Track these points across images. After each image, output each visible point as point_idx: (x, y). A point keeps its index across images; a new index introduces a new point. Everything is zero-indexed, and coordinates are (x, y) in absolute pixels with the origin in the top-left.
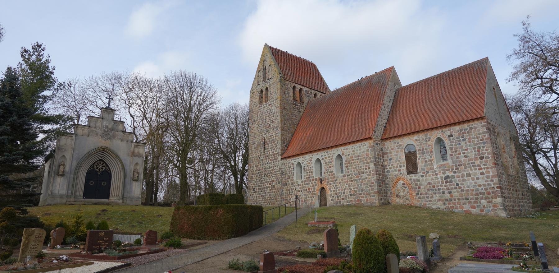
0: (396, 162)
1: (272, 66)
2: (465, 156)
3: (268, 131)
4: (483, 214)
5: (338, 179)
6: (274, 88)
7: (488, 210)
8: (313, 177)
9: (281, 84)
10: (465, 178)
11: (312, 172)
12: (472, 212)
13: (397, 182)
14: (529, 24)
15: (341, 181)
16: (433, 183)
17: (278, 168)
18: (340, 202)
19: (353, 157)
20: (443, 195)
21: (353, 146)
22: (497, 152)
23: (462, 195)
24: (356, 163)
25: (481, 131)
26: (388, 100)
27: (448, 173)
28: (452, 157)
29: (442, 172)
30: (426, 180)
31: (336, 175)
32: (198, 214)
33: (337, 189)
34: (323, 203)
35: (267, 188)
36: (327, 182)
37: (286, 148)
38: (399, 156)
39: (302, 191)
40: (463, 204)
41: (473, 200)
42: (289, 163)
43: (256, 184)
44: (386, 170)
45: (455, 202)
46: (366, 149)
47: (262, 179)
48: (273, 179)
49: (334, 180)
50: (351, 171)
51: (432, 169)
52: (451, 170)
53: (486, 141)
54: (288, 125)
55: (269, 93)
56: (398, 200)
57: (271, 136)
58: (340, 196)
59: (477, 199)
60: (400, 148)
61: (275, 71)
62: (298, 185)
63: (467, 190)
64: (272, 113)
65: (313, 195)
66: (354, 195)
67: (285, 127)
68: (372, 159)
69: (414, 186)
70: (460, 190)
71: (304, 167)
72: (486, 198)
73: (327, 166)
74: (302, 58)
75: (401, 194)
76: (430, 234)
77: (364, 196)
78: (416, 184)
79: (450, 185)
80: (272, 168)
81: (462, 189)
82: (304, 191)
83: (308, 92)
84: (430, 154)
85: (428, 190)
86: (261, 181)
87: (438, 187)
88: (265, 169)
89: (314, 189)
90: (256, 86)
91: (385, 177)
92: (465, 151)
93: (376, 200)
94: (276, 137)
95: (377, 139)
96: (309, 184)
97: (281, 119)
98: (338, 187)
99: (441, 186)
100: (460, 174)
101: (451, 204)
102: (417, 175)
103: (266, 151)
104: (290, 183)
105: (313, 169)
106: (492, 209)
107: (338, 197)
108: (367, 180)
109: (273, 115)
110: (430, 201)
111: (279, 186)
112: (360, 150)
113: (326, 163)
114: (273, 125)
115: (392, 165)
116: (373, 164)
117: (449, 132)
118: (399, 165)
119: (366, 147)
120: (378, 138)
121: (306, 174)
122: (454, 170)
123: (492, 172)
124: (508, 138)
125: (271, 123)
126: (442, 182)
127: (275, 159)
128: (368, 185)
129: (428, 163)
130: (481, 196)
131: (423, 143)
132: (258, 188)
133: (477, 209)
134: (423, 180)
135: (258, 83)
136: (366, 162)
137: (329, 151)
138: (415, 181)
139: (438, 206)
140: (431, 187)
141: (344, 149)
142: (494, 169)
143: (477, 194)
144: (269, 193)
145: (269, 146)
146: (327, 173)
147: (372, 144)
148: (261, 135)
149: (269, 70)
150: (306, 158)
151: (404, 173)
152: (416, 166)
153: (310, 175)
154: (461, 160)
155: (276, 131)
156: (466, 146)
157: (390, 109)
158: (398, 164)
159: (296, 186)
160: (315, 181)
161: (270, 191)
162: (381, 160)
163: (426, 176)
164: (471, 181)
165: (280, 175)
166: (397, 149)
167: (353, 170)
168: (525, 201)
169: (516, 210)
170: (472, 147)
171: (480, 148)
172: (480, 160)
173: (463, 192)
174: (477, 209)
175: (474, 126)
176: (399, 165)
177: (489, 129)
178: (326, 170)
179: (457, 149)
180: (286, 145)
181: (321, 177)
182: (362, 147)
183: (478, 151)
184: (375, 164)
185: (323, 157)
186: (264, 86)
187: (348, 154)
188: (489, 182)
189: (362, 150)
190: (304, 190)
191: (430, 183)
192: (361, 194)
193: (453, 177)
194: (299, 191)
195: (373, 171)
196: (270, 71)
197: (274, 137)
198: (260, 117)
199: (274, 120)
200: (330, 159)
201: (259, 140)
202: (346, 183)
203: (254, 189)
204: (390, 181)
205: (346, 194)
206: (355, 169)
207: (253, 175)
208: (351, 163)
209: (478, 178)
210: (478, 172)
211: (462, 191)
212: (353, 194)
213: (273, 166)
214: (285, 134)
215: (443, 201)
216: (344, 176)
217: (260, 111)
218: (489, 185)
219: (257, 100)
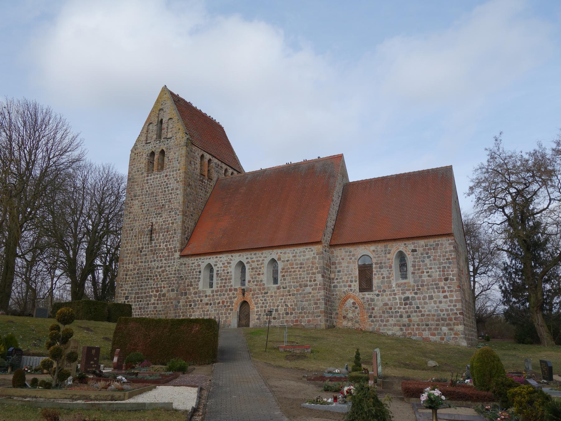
0: (346, 275)
2: (429, 276)
3: (159, 214)
4: (443, 343)
5: (269, 292)
6: (175, 153)
7: (449, 338)
8: (231, 286)
9: (188, 149)
10: (427, 301)
11: (230, 279)
12: (432, 340)
13: (345, 301)
14: (501, 140)
15: (273, 294)
16: (389, 304)
17: (174, 269)
18: (270, 322)
20: (400, 319)
21: (294, 250)
23: (422, 320)
24: (297, 272)
25: (447, 250)
27: (408, 294)
29: (401, 292)
30: (382, 301)
31: (266, 286)
34: (244, 322)
35: (151, 296)
36: (253, 295)
38: (350, 268)
39: (211, 304)
40: (423, 331)
41: (434, 327)
42: (193, 264)
43: (132, 290)
45: (414, 328)
46: (313, 255)
47: (142, 283)
49: (263, 292)
50: (290, 282)
51: (390, 287)
52: (411, 291)
55: (166, 159)
56: (345, 323)
57: (164, 222)
59: (438, 325)
60: (353, 258)
61: (179, 129)
62: (206, 296)
63: (428, 315)
65: (229, 311)
66: (292, 314)
67: (188, 212)
68: (319, 269)
70: (420, 314)
72: (448, 325)
73: (254, 273)
74: (208, 115)
75: (350, 315)
76: (428, 362)
77: (305, 316)
78: (369, 305)
80: (163, 269)
81: (423, 313)
83: (218, 165)
84: (389, 270)
85: (384, 312)
86: (141, 286)
87: (396, 309)
88: (150, 268)
89: (232, 303)
91: (331, 292)
92: (429, 270)
94: (173, 223)
96: (224, 295)
97: (184, 199)
98: (268, 301)
99: (399, 308)
100: (422, 296)
101: (409, 330)
102: (372, 293)
103: (153, 242)
105: (231, 275)
106: (453, 338)
108: (310, 295)
109: (170, 192)
110: (385, 325)
111: (172, 295)
113: (252, 269)
114: (169, 207)
115: (341, 278)
116: (320, 275)
117: (413, 246)
118: (350, 279)
119: (312, 253)
120: (327, 244)
122: (415, 290)
126: (401, 304)
127: (169, 256)
128: (312, 302)
129: (386, 280)
130: (443, 322)
131: (381, 256)
132: (133, 296)
133: (437, 336)
134: (378, 300)
135: (147, 140)
136: (311, 272)
137: (259, 253)
138: (368, 301)
139: (393, 332)
140: (388, 309)
141: (281, 253)
142: (458, 293)
143: (438, 320)
144: (154, 304)
145: (159, 236)
146: (253, 282)
148: (147, 219)
150: (222, 259)
151: (355, 290)
153: (225, 283)
154: (424, 280)
156: (430, 264)
157: (338, 208)
158: (348, 278)
159: (202, 297)
160: (233, 291)
161: (156, 302)
164: (433, 304)
165: (176, 280)
166: (348, 260)
167: (292, 281)
170: (437, 266)
171: (445, 268)
172: (444, 282)
173: (424, 316)
174: (437, 336)
176: (349, 280)
178: (252, 278)
179: (420, 266)
180: (187, 240)
181: (243, 287)
182: (307, 252)
183: (443, 271)
184: (323, 276)
185: (248, 260)
188: (452, 307)
189: (307, 257)
190: (215, 304)
191: (386, 304)
192: (301, 313)
193: (413, 298)
194: (207, 304)
195: (319, 285)
197: (169, 224)
198: (147, 191)
199: (172, 198)
200: (259, 263)
201: (143, 225)
202: (280, 298)
204: (337, 298)
205: (279, 312)
206: (295, 280)
208: (290, 272)
209: (440, 302)
210: (441, 295)
211: (423, 315)
212: (289, 312)
213: (164, 265)
215: (400, 326)
216: (278, 288)
217: (147, 183)
218: (452, 310)
219: (143, 165)
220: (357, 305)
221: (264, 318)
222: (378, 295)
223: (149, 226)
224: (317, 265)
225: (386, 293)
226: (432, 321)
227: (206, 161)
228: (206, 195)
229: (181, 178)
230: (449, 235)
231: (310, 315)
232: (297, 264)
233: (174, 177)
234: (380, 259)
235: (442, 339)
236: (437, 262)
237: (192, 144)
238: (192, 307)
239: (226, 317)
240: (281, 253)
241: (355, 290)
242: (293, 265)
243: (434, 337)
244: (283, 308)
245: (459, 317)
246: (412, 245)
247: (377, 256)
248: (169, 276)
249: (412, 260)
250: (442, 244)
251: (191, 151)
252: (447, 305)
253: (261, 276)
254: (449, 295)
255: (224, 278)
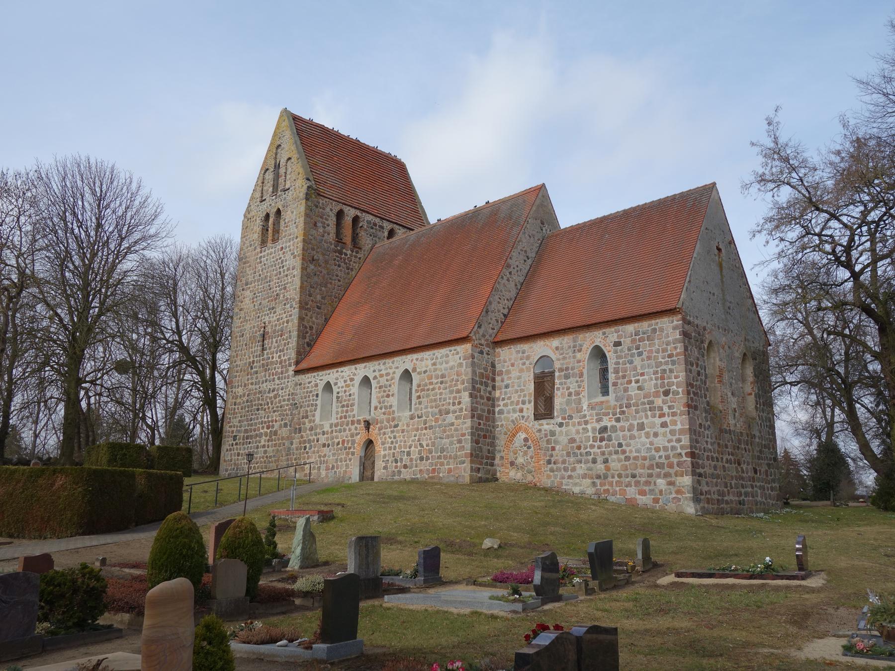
1: (292, 160)
2: (639, 388)
3: (273, 308)
5: (400, 424)
6: (292, 212)
7: (666, 500)
9: (309, 203)
10: (635, 432)
11: (353, 405)
12: (639, 502)
13: (514, 435)
14: (778, 123)
15: (405, 427)
17: (288, 393)
18: (400, 472)
19: (431, 378)
20: (592, 465)
21: (434, 354)
22: (698, 383)
25: (670, 339)
26: (522, 257)
27: (607, 422)
28: (615, 389)
29: (595, 418)
30: (567, 435)
31: (396, 415)
32: (14, 483)
33: (397, 445)
35: (260, 435)
36: (380, 429)
37: (308, 349)
38: (523, 380)
41: (644, 479)
42: (309, 383)
44: (497, 409)
45: (613, 482)
46: (459, 361)
47: (252, 415)
48: (275, 416)
49: (393, 424)
50: (426, 407)
51: (579, 410)
52: (611, 416)
53: (676, 358)
54: (319, 297)
55: (282, 223)
57: (278, 320)
58: (401, 459)
59: (650, 475)
61: (299, 174)
63: (636, 458)
64: (285, 268)
65: (350, 456)
66: (428, 458)
67: (310, 303)
69: (544, 445)
70: (623, 457)
71: (338, 393)
72: (666, 475)
73: (382, 393)
75: (520, 460)
78: (548, 442)
79: (607, 446)
81: (627, 454)
82: (333, 446)
83: (375, 225)
84: (579, 380)
88: (260, 392)
89: (353, 442)
90: (258, 203)
92: (639, 377)
93: (464, 471)
94: (288, 322)
95: (483, 342)
96: (345, 430)
97: (302, 283)
98: (399, 439)
99: (592, 447)
101: (605, 485)
102: (552, 421)
104: (308, 428)
105: (354, 399)
107: (396, 461)
108: (453, 428)
110: (570, 477)
111: (284, 432)
112: (447, 363)
113: (380, 387)
114: (284, 296)
116: (467, 394)
117: (615, 335)
118: (522, 398)
120: (487, 340)
121: (340, 410)
122: (616, 414)
123: (681, 423)
124: (737, 354)
125: (280, 290)
127: (282, 373)
128: (455, 438)
129: (574, 397)
130: (658, 470)
132: (242, 434)
135: (262, 197)
136: (455, 388)
137: (389, 361)
138: (546, 435)
139: (582, 488)
140: (575, 448)
142: (684, 416)
143: (651, 467)
144: (264, 446)
146: (381, 408)
147: (470, 351)
148: (259, 317)
149: (286, 169)
150: (344, 373)
151: (529, 416)
152: (551, 403)
153: (347, 411)
155: (290, 309)
156: (642, 367)
160: (356, 425)
161: (267, 443)
162: (487, 386)
163: (566, 426)
164: (644, 439)
165: (290, 409)
168: (758, 484)
169: (727, 502)
171: (666, 373)
175: (660, 325)
176: (520, 400)
177: (685, 334)
178: (380, 403)
179: (626, 371)
181: (368, 418)
182: (450, 356)
183: (662, 378)
184: (471, 395)
186: (273, 205)
187: (424, 369)
188: (674, 444)
189: (451, 364)
191: (572, 441)
192: (439, 457)
194: (324, 445)
195: (466, 410)
196: (288, 173)
197: (283, 324)
198: (260, 275)
199: (287, 283)
201: (254, 327)
203: (235, 438)
206: (434, 404)
207: (235, 405)
208: (428, 390)
210: (656, 422)
211: (627, 459)
214: (308, 318)
216: (412, 418)
217: (261, 262)
218: (673, 448)
219: (256, 236)
220: (530, 442)
221: (392, 466)
222: (561, 425)
223: (261, 328)
224: (464, 377)
225: (574, 420)
226: (641, 469)
227: (348, 220)
228: (348, 273)
229: (298, 251)
230: (670, 312)
231: (451, 461)
232: (437, 377)
233: (290, 250)
234: (566, 361)
235: (656, 501)
236: (653, 362)
237: (319, 195)
238: (307, 450)
239: (346, 465)
240: (417, 359)
241: (529, 416)
242: (432, 378)
243: (644, 497)
244: (417, 450)
245: (685, 461)
246: (615, 334)
247: (561, 356)
248: (283, 403)
249: (614, 361)
250: (662, 330)
251: (317, 207)
252: (666, 439)
253: (391, 398)
254: (670, 421)
255: (345, 403)
